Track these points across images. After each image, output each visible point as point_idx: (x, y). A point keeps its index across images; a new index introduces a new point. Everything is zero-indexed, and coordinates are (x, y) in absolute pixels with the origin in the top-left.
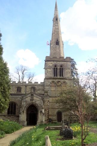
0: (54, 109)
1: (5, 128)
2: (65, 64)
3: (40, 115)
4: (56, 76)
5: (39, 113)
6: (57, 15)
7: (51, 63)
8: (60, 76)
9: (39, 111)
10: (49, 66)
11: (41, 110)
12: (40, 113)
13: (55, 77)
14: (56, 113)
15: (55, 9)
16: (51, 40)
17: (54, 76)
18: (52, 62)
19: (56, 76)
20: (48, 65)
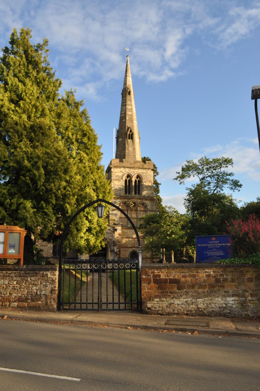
0: (125, 247)
1: (92, 137)
2: (143, 173)
3: (111, 256)
4: (129, 193)
5: (109, 253)
6: (147, 313)
7: (121, 172)
8: (135, 194)
9: (109, 250)
10: (117, 176)
11: (112, 247)
12: (111, 253)
13: (126, 195)
14: (128, 255)
15: (121, 107)
16: (118, 129)
17: (126, 193)
18: (122, 169)
19: (129, 193)
20: (116, 174)
